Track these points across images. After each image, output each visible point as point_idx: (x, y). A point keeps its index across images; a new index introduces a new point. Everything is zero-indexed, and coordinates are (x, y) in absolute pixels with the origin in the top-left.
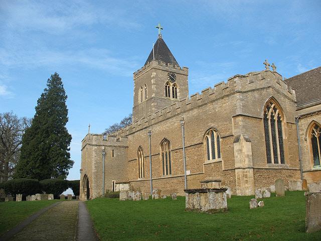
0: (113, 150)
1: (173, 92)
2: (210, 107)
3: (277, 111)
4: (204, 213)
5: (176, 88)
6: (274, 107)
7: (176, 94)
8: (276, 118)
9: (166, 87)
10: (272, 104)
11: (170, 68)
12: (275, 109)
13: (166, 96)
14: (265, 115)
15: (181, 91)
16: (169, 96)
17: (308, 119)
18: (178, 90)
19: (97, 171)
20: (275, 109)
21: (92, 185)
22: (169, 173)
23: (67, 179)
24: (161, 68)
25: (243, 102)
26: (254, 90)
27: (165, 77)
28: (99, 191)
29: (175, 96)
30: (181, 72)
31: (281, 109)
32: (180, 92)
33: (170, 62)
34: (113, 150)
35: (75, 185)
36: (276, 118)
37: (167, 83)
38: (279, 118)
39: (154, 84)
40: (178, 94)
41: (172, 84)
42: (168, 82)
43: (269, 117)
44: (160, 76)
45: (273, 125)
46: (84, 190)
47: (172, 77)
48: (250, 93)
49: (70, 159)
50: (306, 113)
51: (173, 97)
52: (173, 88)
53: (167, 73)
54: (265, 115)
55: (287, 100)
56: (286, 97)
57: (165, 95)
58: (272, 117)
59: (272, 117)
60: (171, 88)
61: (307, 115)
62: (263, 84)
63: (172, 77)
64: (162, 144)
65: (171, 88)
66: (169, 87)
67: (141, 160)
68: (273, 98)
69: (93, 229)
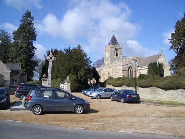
0: (136, 63)
2: (117, 67)
4: (31, 44)
8: (131, 70)
11: (116, 47)
12: (131, 68)
14: (128, 70)
18: (118, 54)
20: (131, 68)
24: (113, 47)
27: (114, 50)
34: (136, 63)
36: (131, 70)
37: (115, 52)
38: (132, 70)
39: (46, 89)
41: (116, 52)
43: (129, 70)
45: (130, 72)
47: (116, 50)
54: (128, 70)
58: (130, 70)
59: (130, 70)
62: (129, 63)
63: (116, 50)
64: (108, 73)
67: (104, 77)
69: (74, 3)
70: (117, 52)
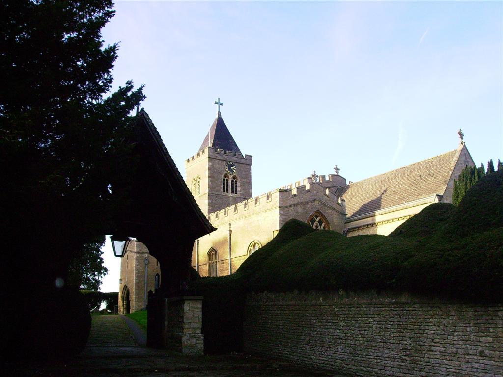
1: (232, 186)
3: (323, 224)
5: (236, 181)
6: (320, 220)
7: (236, 189)
9: (224, 180)
10: (317, 217)
11: (229, 156)
13: (224, 191)
15: (243, 184)
16: (227, 192)
17: (355, 233)
18: (238, 184)
19: (139, 281)
21: (133, 297)
22: (230, 190)
23: (101, 291)
24: (218, 156)
25: (284, 217)
26: (296, 204)
28: (141, 304)
29: (234, 190)
30: (243, 161)
31: (328, 223)
32: (241, 186)
33: (230, 149)
35: (111, 298)
37: (226, 176)
40: (239, 189)
41: (231, 177)
42: (226, 174)
44: (217, 166)
46: (123, 303)
48: (292, 208)
49: (103, 265)
50: (353, 227)
51: (233, 192)
52: (232, 181)
53: (225, 163)
55: (335, 213)
56: (334, 209)
57: (222, 190)
60: (230, 181)
61: (363, 226)
65: (230, 181)
66: (227, 180)
68: (318, 211)
70: (234, 178)
